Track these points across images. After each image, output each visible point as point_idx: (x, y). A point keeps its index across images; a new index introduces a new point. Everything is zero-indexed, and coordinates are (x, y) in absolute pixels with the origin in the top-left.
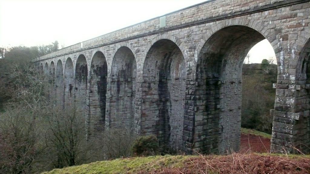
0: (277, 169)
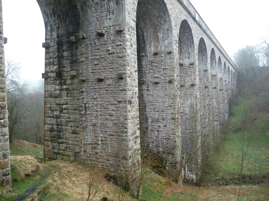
0: (58, 191)
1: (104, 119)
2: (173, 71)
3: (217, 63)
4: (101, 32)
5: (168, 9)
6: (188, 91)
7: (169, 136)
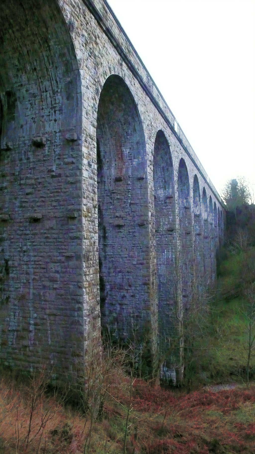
1: (41, 287)
2: (146, 208)
3: (201, 197)
4: (39, 141)
5: (140, 112)
6: (163, 239)
7: (139, 313)
